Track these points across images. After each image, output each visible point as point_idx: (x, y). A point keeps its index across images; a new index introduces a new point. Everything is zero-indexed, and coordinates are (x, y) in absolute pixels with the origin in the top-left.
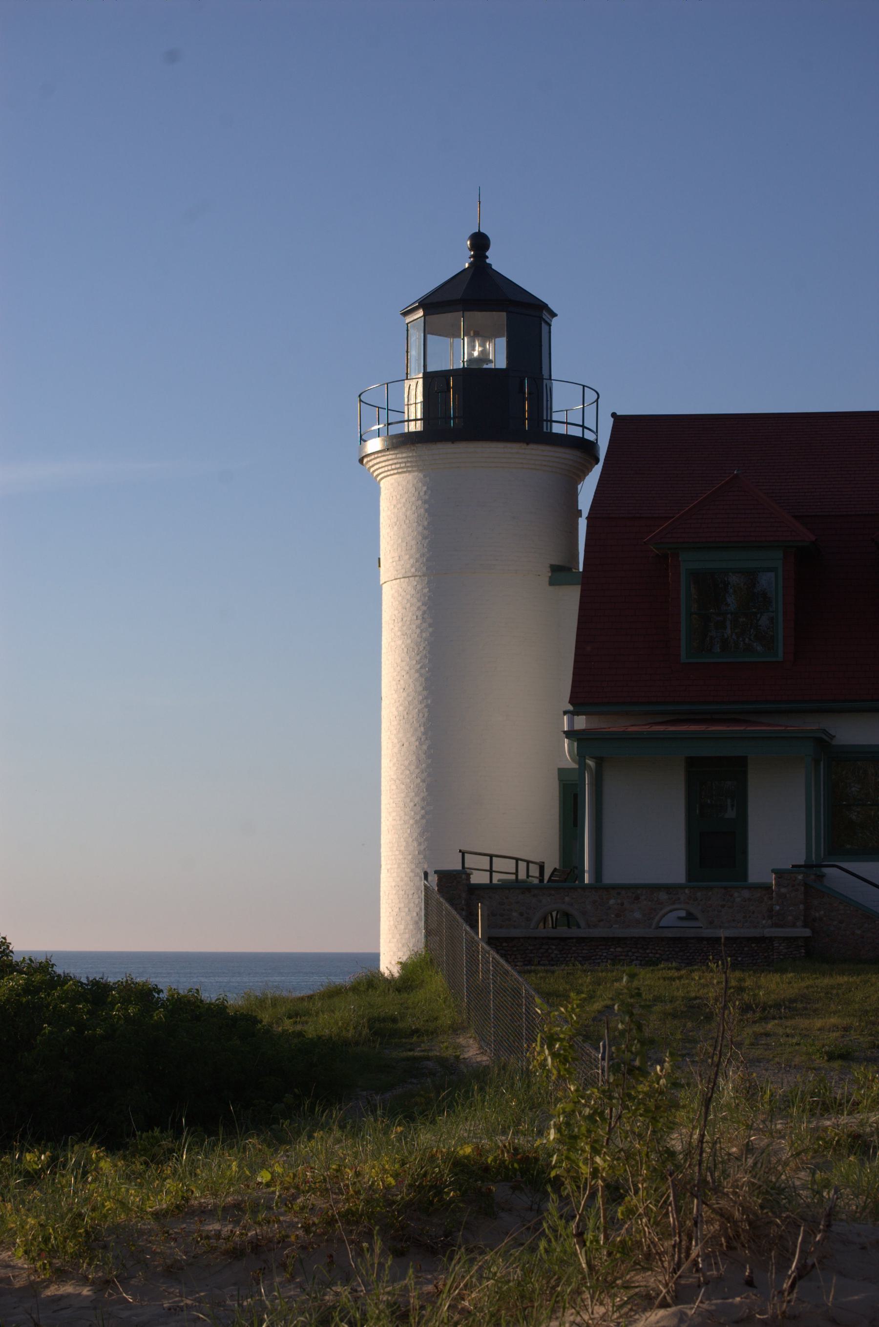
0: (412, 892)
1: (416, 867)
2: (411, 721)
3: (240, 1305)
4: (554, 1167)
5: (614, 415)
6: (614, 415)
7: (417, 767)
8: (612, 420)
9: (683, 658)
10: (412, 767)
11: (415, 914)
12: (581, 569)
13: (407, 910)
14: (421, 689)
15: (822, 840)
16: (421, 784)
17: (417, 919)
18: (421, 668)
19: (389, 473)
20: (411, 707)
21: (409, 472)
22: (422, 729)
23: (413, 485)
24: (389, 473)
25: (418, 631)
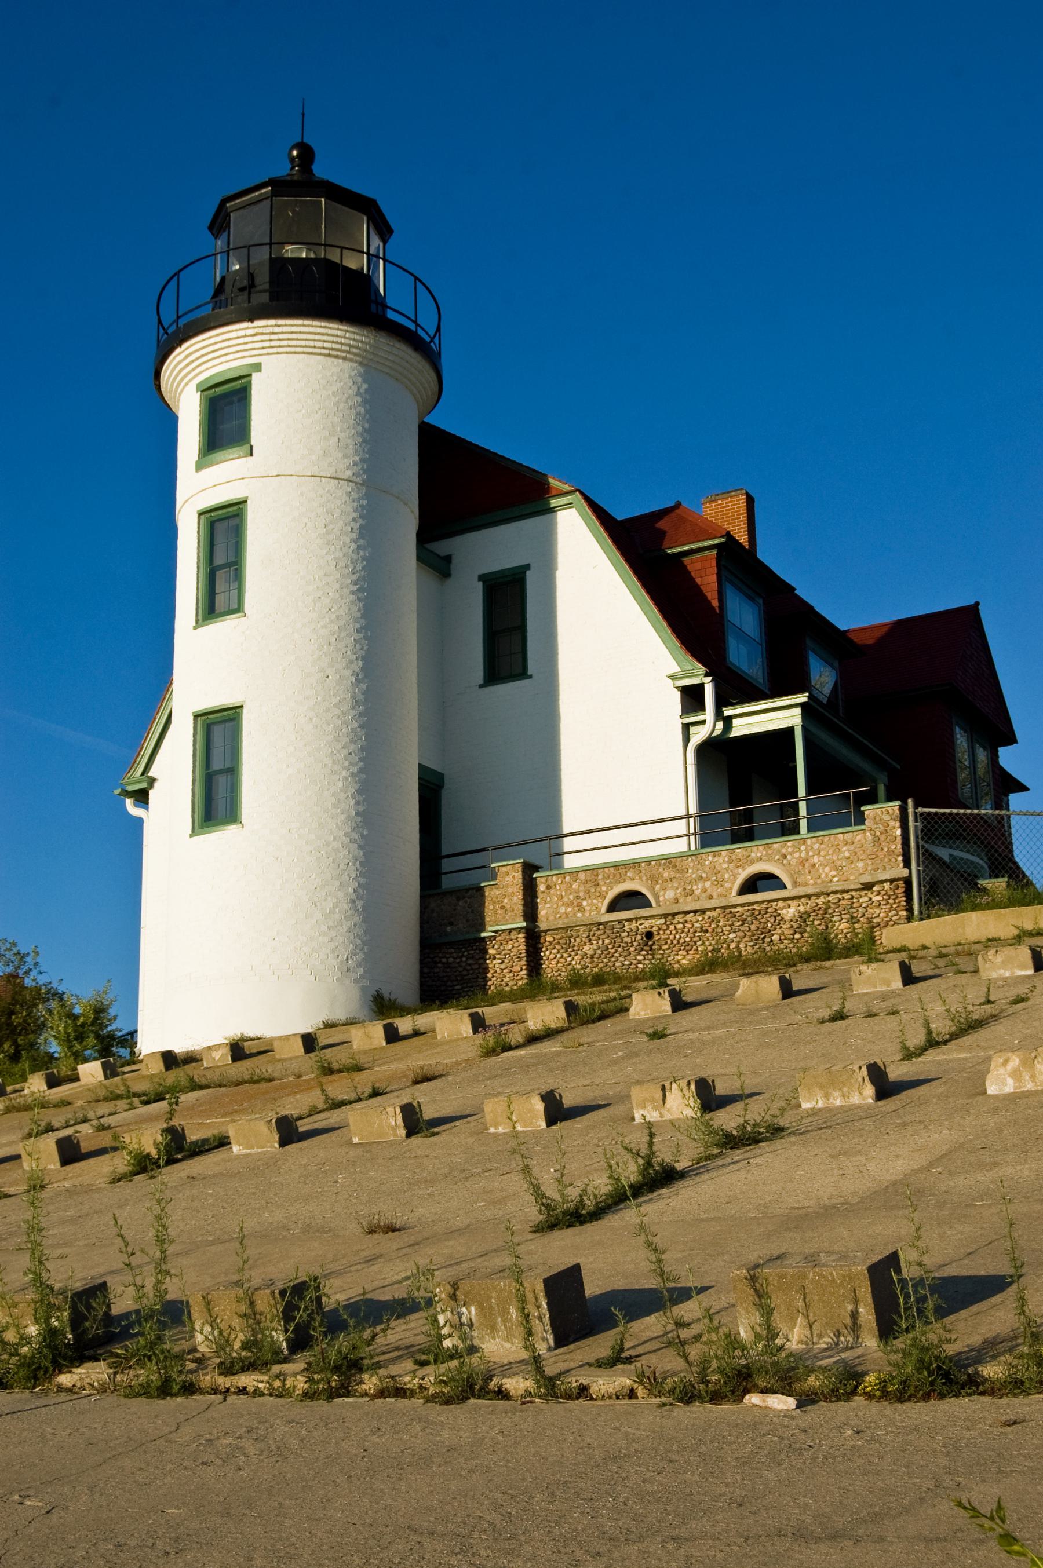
0: (347, 861)
1: (353, 831)
2: (344, 651)
3: (654, 1498)
4: (159, 1159)
5: (977, 604)
6: (977, 604)
7: (353, 708)
8: (973, 603)
9: (323, 199)
10: (346, 707)
11: (350, 890)
12: (670, 551)
13: (337, 883)
14: (359, 615)
15: (237, 201)
16: (359, 729)
17: (354, 896)
18: (358, 590)
19: (306, 350)
20: (343, 634)
21: (345, 359)
22: (360, 663)
23: (350, 377)
24: (306, 350)
25: (353, 546)
